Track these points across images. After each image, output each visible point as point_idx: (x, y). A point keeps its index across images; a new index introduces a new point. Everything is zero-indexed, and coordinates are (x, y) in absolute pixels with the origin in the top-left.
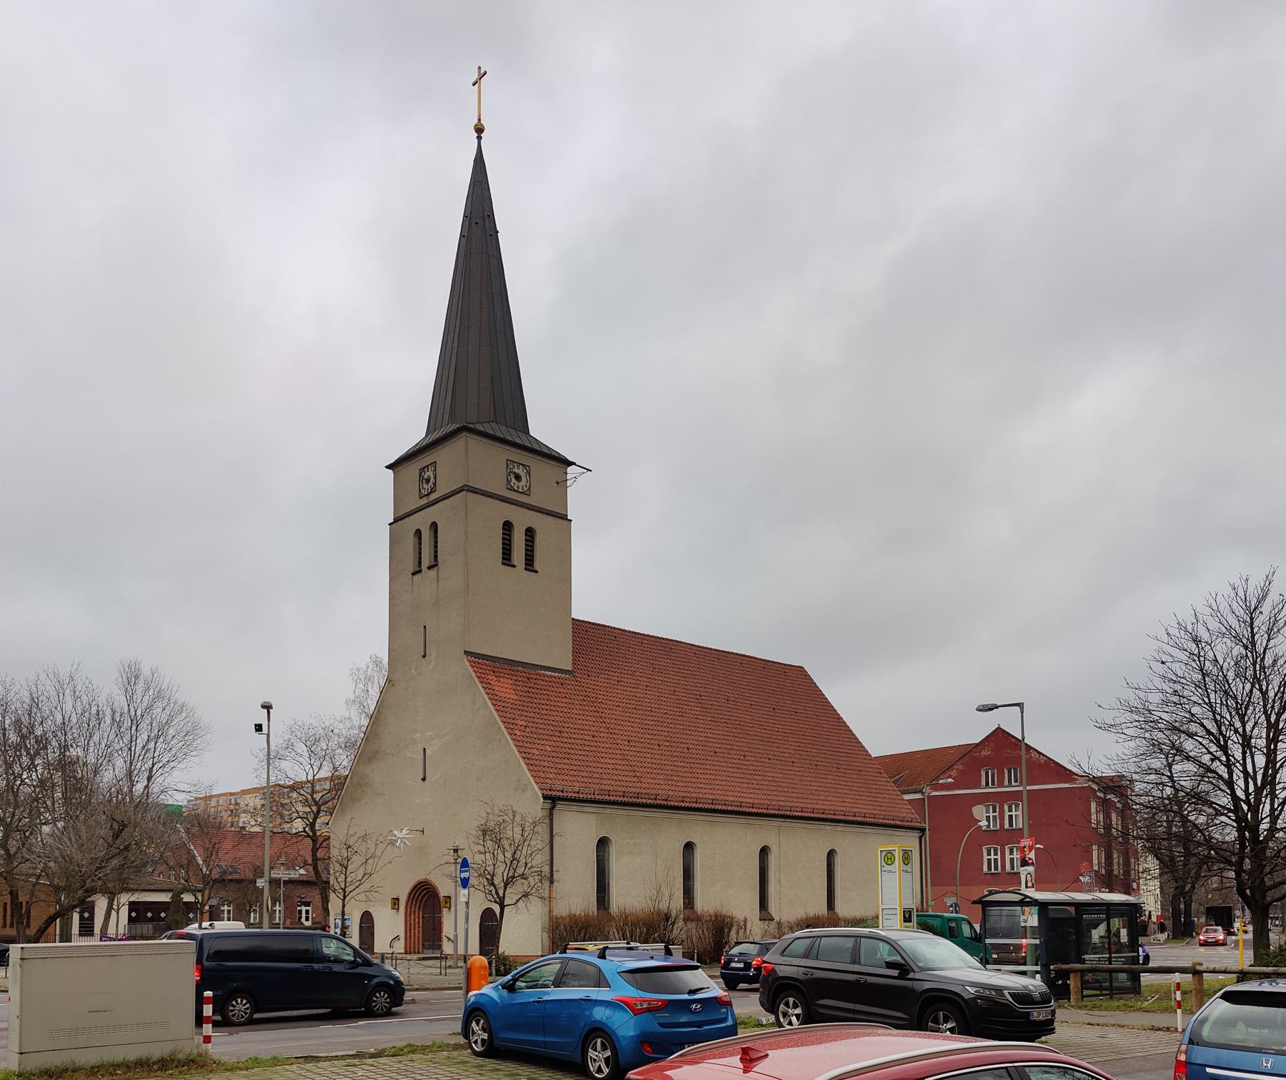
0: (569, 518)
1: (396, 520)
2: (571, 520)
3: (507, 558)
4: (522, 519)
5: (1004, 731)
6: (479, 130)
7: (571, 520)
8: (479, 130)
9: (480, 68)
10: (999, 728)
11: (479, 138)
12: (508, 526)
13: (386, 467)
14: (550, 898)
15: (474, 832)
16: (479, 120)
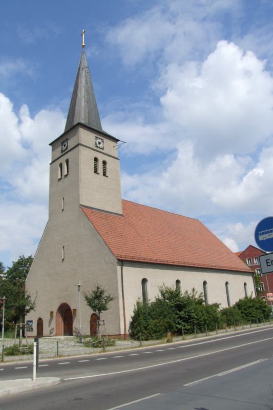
1: (53, 162)
3: (96, 171)
4: (101, 158)
5: (252, 246)
10: (250, 246)
12: (96, 160)
15: (91, 293)
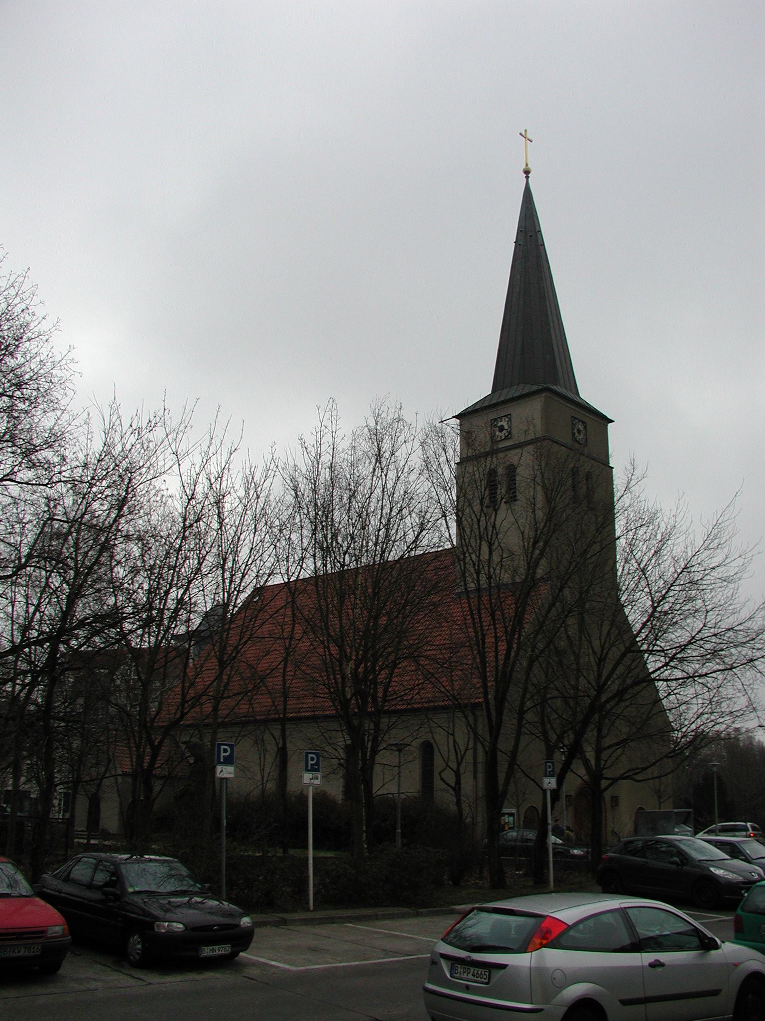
0: (611, 465)
2: (613, 468)
6: (527, 172)
7: (613, 468)
8: (527, 172)
9: (521, 134)
11: (527, 177)
13: (613, 421)
14: (283, 721)
16: (527, 165)
